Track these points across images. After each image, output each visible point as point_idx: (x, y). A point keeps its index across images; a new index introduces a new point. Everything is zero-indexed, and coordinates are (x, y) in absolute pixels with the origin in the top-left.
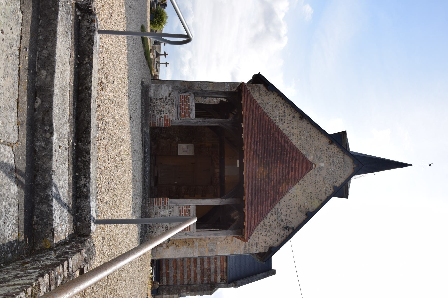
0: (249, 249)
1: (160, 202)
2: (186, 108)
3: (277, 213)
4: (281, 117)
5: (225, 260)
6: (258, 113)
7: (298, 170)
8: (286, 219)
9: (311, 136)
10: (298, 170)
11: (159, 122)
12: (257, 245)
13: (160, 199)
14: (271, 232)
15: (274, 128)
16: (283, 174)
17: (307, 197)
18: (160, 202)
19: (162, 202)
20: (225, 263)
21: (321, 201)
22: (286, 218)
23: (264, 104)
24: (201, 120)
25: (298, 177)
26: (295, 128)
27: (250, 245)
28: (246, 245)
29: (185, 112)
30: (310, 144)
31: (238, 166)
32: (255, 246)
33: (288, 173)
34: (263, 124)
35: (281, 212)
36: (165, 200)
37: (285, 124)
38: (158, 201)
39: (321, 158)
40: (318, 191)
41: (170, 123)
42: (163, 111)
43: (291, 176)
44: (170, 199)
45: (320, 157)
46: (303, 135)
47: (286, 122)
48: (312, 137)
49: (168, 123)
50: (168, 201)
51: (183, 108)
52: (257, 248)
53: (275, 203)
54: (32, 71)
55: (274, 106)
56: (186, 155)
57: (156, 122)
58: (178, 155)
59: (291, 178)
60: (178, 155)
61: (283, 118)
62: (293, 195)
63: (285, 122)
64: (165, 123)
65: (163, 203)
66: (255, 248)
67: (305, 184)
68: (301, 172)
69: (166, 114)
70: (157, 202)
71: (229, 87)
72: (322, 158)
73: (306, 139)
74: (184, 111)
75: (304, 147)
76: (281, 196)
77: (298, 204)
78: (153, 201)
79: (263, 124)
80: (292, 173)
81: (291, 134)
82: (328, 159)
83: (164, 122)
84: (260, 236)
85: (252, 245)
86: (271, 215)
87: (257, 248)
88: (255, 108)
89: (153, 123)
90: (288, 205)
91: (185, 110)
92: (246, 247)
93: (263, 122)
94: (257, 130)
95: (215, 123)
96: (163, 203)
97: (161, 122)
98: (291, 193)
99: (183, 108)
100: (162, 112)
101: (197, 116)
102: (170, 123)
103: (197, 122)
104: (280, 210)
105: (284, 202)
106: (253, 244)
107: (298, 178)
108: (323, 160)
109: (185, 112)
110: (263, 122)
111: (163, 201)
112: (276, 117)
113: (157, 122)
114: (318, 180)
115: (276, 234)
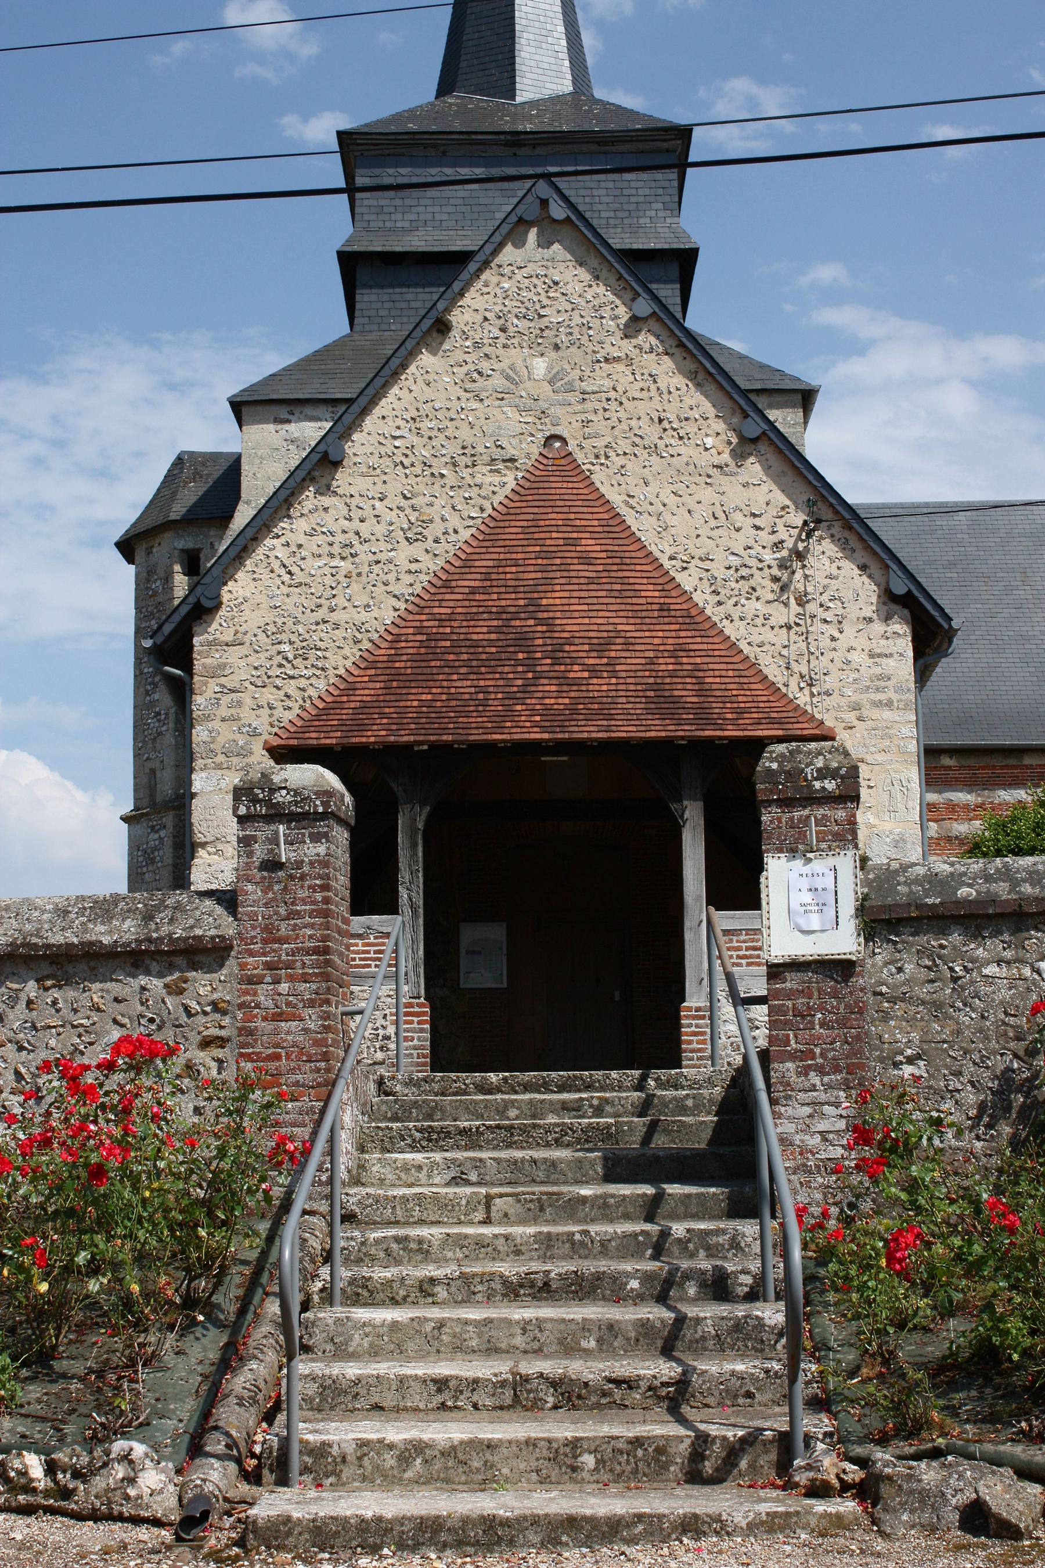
0: (898, 690)
1: (695, 1034)
2: (360, 948)
3: (744, 572)
4: (336, 550)
5: (1012, 762)
6: (371, 685)
7: (572, 516)
8: (774, 532)
9: (414, 414)
10: (572, 516)
11: (416, 1042)
12: (879, 655)
13: (687, 1034)
14: (825, 598)
15: (418, 617)
16: (591, 581)
17: (681, 438)
18: (695, 1034)
19: (693, 1029)
20: (1028, 761)
21: (696, 372)
22: (769, 529)
23: (280, 621)
24: (403, 893)
25: (601, 516)
26: (380, 488)
27: (882, 684)
28: (880, 701)
29: (375, 952)
30: (452, 420)
31: (565, 758)
32: (884, 661)
33: (587, 560)
34: (409, 664)
35: (742, 552)
36: (687, 1017)
37: (365, 534)
38: (690, 1042)
39: (511, 373)
40: (653, 387)
41: (419, 1005)
42: (377, 1029)
43: (598, 548)
44: (684, 1001)
45: (508, 378)
46: (408, 452)
47: (356, 524)
48: (418, 410)
49: (417, 1009)
50: (689, 1009)
51: (361, 959)
52: (891, 655)
53: (698, 619)
54: (617, 994)
55: (286, 578)
56: (505, 951)
57: (415, 1053)
58: (505, 985)
59: (604, 548)
60: (505, 985)
61: (340, 538)
62: (672, 500)
63: (357, 533)
64: (419, 1023)
65: (697, 1026)
66: (889, 665)
67: (624, 446)
68: (580, 503)
69: (385, 1017)
70: (695, 1046)
71: (213, 772)
72: (512, 367)
73: (430, 438)
74: (372, 955)
75: (464, 448)
76: (674, 593)
77: (709, 476)
78: (692, 1059)
79: (409, 664)
80: (588, 544)
81: (404, 503)
82: (515, 341)
83: (415, 1025)
84: (843, 642)
85: (881, 677)
86: (753, 597)
87: (891, 655)
88: (353, 698)
89: (418, 1064)
90: (713, 523)
91: (368, 952)
92: (889, 704)
93: (402, 664)
94: (434, 690)
95: (414, 846)
96: (697, 1026)
97: (416, 1035)
98: (662, 508)
99: (361, 959)
100: (381, 1032)
101: (392, 908)
102: (419, 1005)
103: (415, 912)
104: (732, 558)
105: (698, 536)
106: (878, 670)
107: (606, 516)
108: (519, 364)
109: (375, 952)
110: (402, 664)
111: (690, 1026)
112: (334, 571)
113: (415, 1048)
114: (607, 384)
115: (835, 572)
